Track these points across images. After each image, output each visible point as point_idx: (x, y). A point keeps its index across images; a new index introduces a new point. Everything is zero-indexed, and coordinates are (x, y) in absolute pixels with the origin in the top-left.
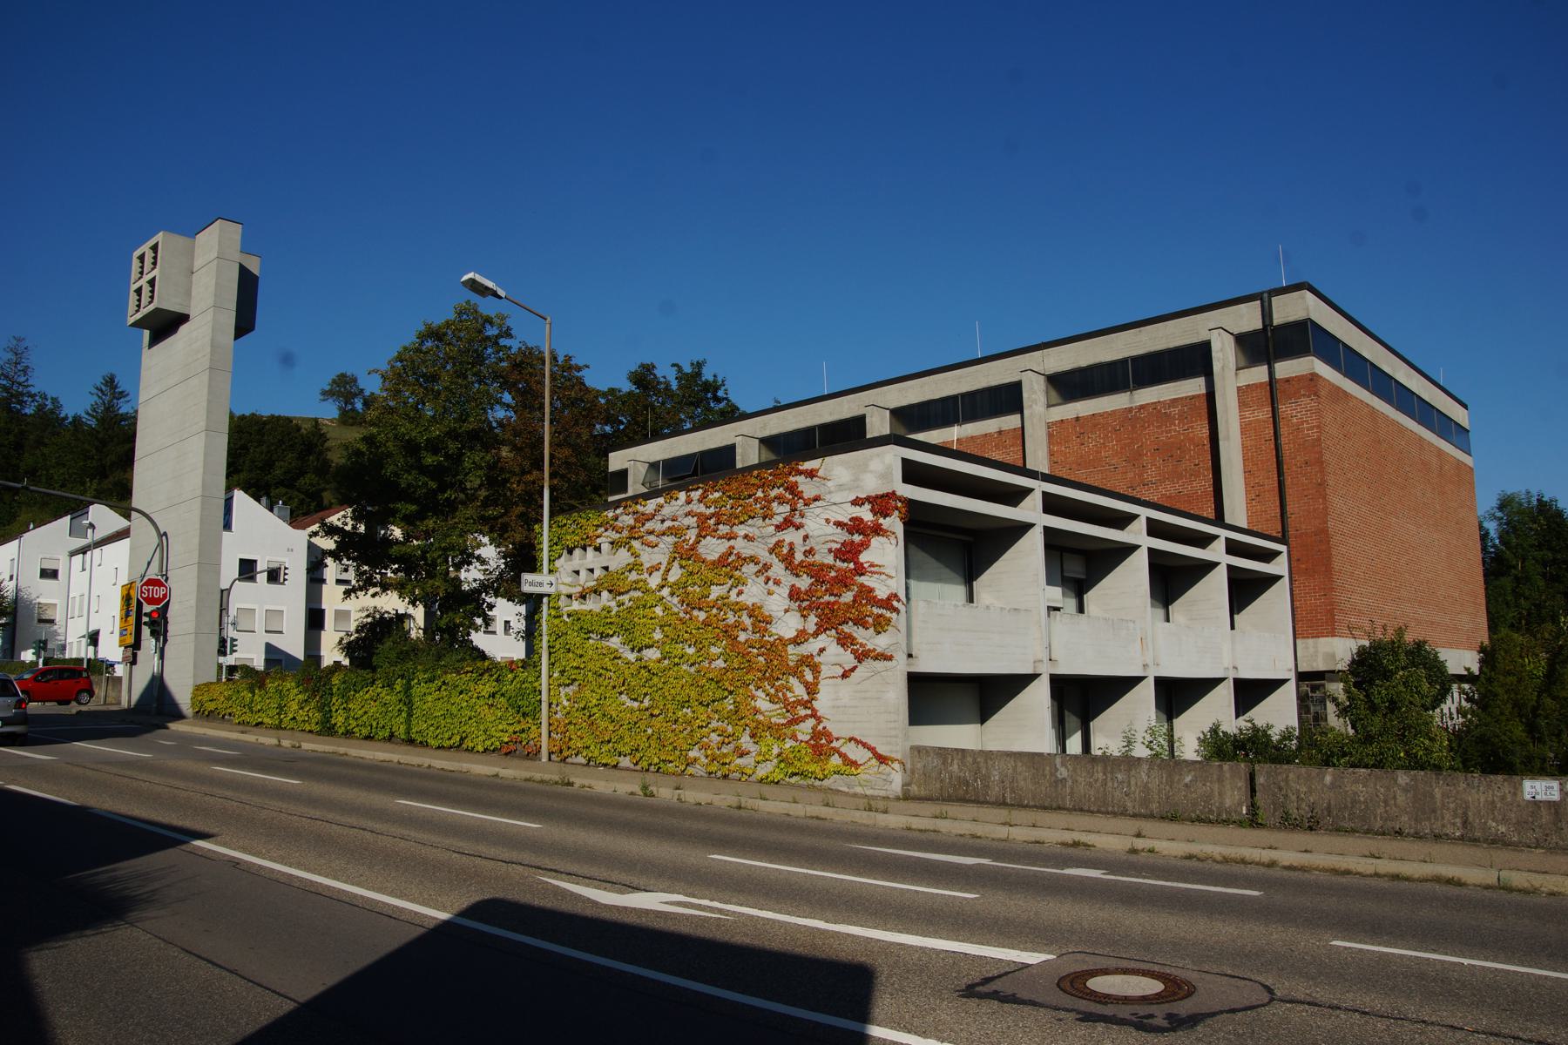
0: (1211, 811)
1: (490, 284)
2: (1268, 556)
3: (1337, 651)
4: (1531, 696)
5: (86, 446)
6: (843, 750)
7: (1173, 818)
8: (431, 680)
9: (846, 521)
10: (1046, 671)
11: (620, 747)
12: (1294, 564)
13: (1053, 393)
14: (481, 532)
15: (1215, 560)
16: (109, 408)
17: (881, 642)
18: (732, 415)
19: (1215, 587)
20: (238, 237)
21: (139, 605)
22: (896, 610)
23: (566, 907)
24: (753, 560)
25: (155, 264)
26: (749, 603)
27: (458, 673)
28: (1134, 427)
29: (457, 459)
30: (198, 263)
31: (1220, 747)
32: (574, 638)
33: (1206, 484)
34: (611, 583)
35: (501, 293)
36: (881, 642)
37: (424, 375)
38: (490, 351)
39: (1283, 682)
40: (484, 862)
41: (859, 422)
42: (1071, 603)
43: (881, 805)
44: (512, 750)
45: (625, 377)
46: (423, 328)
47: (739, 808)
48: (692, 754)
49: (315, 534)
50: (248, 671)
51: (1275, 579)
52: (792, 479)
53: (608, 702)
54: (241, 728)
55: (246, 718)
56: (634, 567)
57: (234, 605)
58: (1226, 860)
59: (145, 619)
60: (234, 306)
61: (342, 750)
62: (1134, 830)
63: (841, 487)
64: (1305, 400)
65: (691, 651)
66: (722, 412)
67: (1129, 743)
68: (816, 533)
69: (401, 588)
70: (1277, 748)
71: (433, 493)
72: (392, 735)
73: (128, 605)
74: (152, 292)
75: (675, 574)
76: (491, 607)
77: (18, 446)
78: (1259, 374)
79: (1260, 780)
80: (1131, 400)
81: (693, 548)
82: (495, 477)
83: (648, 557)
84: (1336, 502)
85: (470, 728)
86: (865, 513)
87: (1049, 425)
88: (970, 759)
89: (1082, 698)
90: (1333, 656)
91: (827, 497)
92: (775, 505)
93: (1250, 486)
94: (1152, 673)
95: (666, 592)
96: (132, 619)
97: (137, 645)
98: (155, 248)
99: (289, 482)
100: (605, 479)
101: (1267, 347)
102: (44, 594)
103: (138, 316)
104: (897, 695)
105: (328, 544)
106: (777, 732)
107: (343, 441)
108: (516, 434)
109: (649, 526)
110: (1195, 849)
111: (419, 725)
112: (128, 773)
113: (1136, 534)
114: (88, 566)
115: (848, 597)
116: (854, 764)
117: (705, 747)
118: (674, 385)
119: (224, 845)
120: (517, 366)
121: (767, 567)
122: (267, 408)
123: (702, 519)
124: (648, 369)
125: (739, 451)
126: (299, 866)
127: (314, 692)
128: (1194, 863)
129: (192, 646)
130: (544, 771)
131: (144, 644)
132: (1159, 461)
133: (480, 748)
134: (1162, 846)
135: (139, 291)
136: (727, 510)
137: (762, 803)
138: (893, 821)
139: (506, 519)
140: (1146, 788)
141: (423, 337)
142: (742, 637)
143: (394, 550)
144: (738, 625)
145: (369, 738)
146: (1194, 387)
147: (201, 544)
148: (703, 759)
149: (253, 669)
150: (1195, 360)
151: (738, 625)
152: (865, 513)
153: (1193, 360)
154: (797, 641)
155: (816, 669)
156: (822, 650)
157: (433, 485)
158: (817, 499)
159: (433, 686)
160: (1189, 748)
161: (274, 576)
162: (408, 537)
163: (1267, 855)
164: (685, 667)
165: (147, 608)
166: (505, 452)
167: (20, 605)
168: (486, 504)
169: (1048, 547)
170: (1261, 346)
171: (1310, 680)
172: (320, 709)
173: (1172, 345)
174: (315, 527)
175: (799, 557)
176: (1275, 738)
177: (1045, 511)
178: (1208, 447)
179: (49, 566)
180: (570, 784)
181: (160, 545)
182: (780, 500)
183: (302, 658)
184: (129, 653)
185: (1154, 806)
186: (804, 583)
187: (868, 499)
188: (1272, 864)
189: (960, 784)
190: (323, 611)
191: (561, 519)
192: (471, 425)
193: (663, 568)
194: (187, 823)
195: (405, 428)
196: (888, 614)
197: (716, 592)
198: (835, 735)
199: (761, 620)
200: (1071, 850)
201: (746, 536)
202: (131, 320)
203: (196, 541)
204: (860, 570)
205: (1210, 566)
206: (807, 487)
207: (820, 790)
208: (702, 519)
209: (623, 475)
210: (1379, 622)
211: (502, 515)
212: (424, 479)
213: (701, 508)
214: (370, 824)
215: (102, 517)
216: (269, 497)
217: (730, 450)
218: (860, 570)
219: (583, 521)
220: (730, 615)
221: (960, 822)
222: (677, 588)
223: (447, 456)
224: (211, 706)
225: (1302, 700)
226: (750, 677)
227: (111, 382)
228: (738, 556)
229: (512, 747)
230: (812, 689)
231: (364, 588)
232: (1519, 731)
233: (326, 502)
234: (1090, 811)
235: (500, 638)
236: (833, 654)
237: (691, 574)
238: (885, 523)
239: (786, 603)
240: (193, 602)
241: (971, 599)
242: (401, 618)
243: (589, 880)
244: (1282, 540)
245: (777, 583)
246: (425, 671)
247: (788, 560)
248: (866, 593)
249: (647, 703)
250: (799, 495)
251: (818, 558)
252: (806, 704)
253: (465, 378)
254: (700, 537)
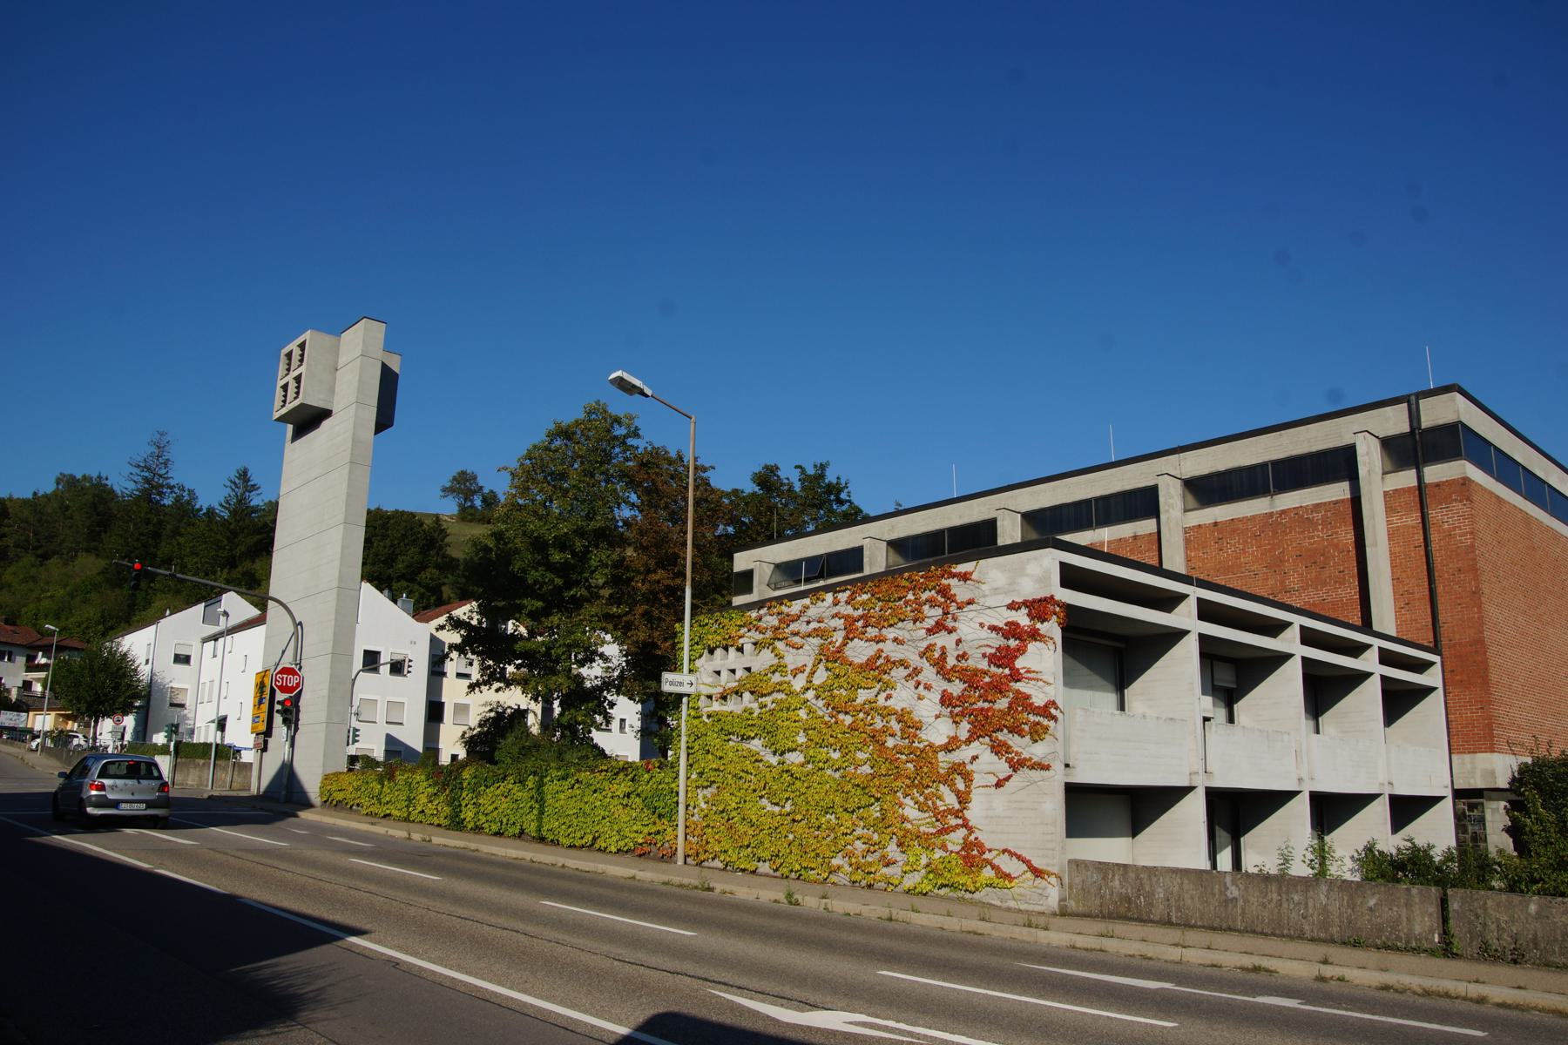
0: (1398, 938)
1: (637, 383)
2: (1421, 666)
3: (1498, 768)
5: (219, 537)
6: (996, 862)
7: (1356, 944)
8: (564, 778)
9: (1001, 625)
10: (1202, 783)
11: (760, 853)
12: (1448, 675)
13: (1190, 498)
14: (603, 629)
16: (241, 501)
17: (1037, 751)
18: (854, 518)
19: (1369, 696)
20: (382, 336)
21: (273, 692)
22: (1054, 718)
23: (746, 1023)
24: (903, 663)
25: (301, 361)
26: (898, 708)
27: (592, 772)
29: (583, 557)
30: (342, 361)
31: (1383, 870)
32: (713, 740)
33: (1353, 592)
34: (754, 685)
35: (648, 391)
36: (1037, 751)
37: (552, 474)
38: (617, 450)
39: (1442, 798)
40: (648, 971)
41: (989, 527)
42: (1221, 713)
43: (1042, 921)
44: (650, 851)
45: (749, 477)
46: (552, 427)
47: (890, 919)
48: (835, 862)
49: (441, 628)
50: (369, 762)
51: (1428, 690)
52: (944, 582)
53: (748, 805)
54: (369, 819)
55: (374, 809)
56: (778, 668)
57: (360, 693)
58: (1427, 993)
59: (278, 707)
60: (375, 402)
61: (473, 846)
62: (1321, 957)
63: (996, 591)
65: (836, 755)
66: (845, 515)
67: (1287, 861)
68: (969, 638)
69: (523, 683)
70: (1439, 869)
71: (558, 590)
72: (522, 832)
73: (262, 692)
74: (298, 388)
75: (821, 677)
76: (612, 705)
77: (156, 535)
78: (1407, 478)
79: (1454, 906)
80: (1272, 505)
81: (839, 650)
82: (620, 578)
83: (792, 659)
84: (1493, 612)
85: (604, 827)
86: (1022, 617)
87: (1186, 531)
88: (1132, 875)
89: (1236, 812)
90: (1492, 773)
91: (982, 601)
92: (926, 608)
93: (1398, 594)
94: (1307, 788)
95: (810, 694)
96: (265, 707)
97: (268, 733)
98: (302, 346)
99: (410, 576)
100: (729, 579)
101: (1415, 450)
102: (175, 678)
103: (284, 411)
104: (1055, 806)
105: (454, 637)
106: (925, 841)
107: (463, 539)
108: (642, 533)
109: (794, 627)
110: (1390, 978)
111: (550, 823)
112: (269, 862)
113: (1288, 642)
114: (220, 653)
115: (1002, 704)
116: (1008, 876)
117: (849, 855)
118: (797, 487)
119: (379, 942)
120: (644, 465)
121: (917, 671)
122: (389, 507)
123: (850, 621)
124: (772, 470)
125: (866, 553)
126: (459, 969)
127: (445, 785)
128: (1389, 995)
129: (322, 735)
130: (680, 874)
131: (275, 731)
133: (614, 849)
134: (1353, 974)
135: (285, 388)
136: (876, 612)
137: (914, 915)
138: (1057, 938)
139: (629, 617)
140: (1325, 910)
141: (552, 436)
142: (890, 743)
143: (519, 646)
144: (885, 730)
145: (498, 834)
146: (1338, 491)
147: (335, 634)
148: (847, 869)
149: (373, 760)
150: (1340, 464)
151: (885, 730)
152: (1022, 617)
153: (1338, 464)
154: (949, 747)
155: (968, 778)
156: (975, 758)
157: (559, 581)
158: (970, 602)
159: (566, 784)
160: (1344, 866)
161: (397, 668)
162: (532, 634)
163: (1474, 990)
164: (829, 772)
165: (280, 696)
166: (630, 552)
167: (154, 688)
168: (613, 600)
169: (1203, 655)
170: (1408, 450)
171: (1469, 799)
172: (450, 804)
173: (1314, 449)
174: (442, 620)
175: (951, 661)
176: (1437, 859)
178: (1353, 553)
179: (183, 651)
180: (710, 889)
181: (295, 633)
182: (932, 603)
183: (420, 749)
184: (261, 740)
185: (1335, 930)
186: (956, 688)
187: (1025, 603)
188: (1481, 1000)
189: (1125, 901)
190: (442, 704)
191: (704, 619)
192: (598, 523)
193: (808, 670)
194: (338, 918)
195: (534, 525)
196: (1045, 722)
197: (863, 696)
198: (988, 846)
199: (910, 726)
200: (1253, 976)
201: (895, 640)
202: (277, 415)
203: (331, 631)
204: (1016, 676)
205: (1363, 676)
206: (960, 590)
207: (973, 903)
208: (850, 621)
209: (748, 576)
210: (1544, 738)
211: (627, 613)
212: (549, 575)
213: (849, 610)
214: (521, 926)
215: (235, 605)
216: (391, 590)
217: (859, 551)
218: (1016, 676)
219: (726, 621)
220: (878, 720)
221: (1127, 942)
222: (821, 691)
223: (574, 554)
224: (340, 796)
225: (1459, 818)
226: (898, 783)
227: (244, 475)
228: (887, 659)
229: (646, 848)
230: (963, 798)
231: (488, 683)
233: (445, 596)
234: (1262, 933)
235: (620, 736)
236: (984, 760)
237: (838, 676)
238: (1043, 628)
239: (938, 708)
240: (325, 692)
241: (1122, 707)
242: (520, 714)
243: (762, 994)
244: (1435, 650)
245: (928, 687)
246: (559, 769)
247: (940, 665)
248: (1022, 700)
249: (788, 808)
250: (952, 599)
251: (971, 663)
252: (957, 814)
253: (592, 476)
254: (847, 639)
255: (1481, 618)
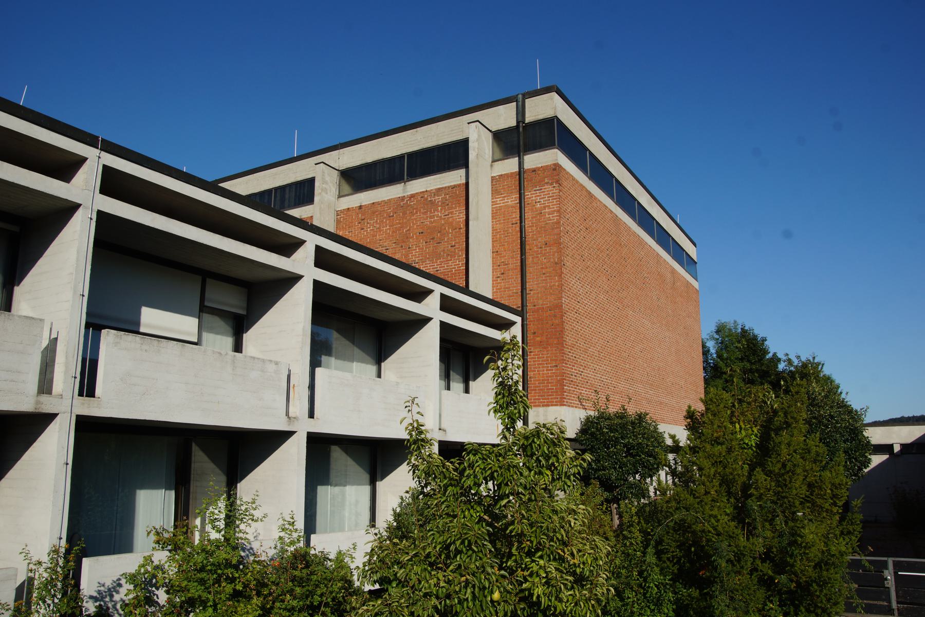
2: (505, 325)
4: (740, 469)
10: (303, 427)
15: (439, 323)
28: (404, 213)
64: (548, 188)
78: (510, 165)
87: (338, 213)
132: (422, 244)
169: (442, 340)
170: (512, 142)
173: (441, 142)
177: (102, 191)
232: (725, 522)
244: (521, 313)
255: (561, 286)
